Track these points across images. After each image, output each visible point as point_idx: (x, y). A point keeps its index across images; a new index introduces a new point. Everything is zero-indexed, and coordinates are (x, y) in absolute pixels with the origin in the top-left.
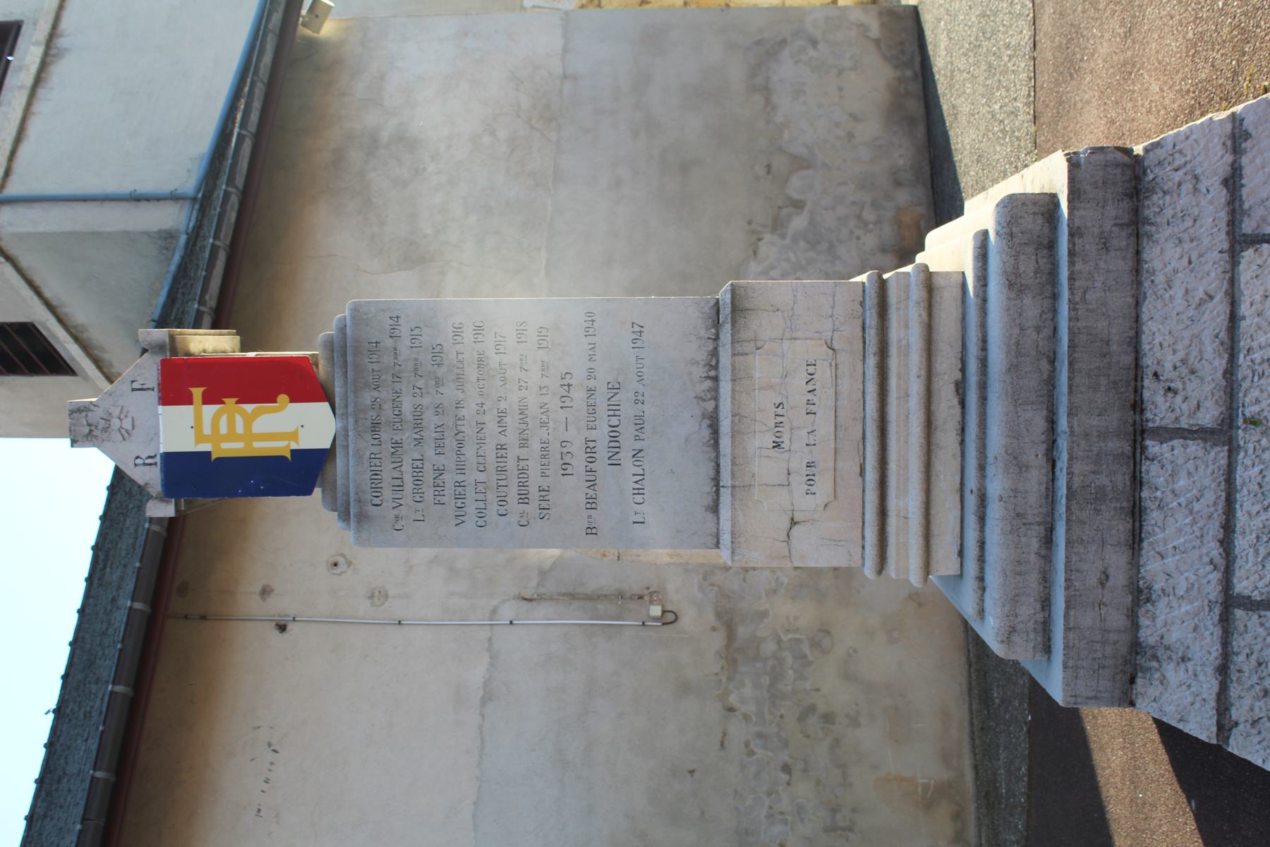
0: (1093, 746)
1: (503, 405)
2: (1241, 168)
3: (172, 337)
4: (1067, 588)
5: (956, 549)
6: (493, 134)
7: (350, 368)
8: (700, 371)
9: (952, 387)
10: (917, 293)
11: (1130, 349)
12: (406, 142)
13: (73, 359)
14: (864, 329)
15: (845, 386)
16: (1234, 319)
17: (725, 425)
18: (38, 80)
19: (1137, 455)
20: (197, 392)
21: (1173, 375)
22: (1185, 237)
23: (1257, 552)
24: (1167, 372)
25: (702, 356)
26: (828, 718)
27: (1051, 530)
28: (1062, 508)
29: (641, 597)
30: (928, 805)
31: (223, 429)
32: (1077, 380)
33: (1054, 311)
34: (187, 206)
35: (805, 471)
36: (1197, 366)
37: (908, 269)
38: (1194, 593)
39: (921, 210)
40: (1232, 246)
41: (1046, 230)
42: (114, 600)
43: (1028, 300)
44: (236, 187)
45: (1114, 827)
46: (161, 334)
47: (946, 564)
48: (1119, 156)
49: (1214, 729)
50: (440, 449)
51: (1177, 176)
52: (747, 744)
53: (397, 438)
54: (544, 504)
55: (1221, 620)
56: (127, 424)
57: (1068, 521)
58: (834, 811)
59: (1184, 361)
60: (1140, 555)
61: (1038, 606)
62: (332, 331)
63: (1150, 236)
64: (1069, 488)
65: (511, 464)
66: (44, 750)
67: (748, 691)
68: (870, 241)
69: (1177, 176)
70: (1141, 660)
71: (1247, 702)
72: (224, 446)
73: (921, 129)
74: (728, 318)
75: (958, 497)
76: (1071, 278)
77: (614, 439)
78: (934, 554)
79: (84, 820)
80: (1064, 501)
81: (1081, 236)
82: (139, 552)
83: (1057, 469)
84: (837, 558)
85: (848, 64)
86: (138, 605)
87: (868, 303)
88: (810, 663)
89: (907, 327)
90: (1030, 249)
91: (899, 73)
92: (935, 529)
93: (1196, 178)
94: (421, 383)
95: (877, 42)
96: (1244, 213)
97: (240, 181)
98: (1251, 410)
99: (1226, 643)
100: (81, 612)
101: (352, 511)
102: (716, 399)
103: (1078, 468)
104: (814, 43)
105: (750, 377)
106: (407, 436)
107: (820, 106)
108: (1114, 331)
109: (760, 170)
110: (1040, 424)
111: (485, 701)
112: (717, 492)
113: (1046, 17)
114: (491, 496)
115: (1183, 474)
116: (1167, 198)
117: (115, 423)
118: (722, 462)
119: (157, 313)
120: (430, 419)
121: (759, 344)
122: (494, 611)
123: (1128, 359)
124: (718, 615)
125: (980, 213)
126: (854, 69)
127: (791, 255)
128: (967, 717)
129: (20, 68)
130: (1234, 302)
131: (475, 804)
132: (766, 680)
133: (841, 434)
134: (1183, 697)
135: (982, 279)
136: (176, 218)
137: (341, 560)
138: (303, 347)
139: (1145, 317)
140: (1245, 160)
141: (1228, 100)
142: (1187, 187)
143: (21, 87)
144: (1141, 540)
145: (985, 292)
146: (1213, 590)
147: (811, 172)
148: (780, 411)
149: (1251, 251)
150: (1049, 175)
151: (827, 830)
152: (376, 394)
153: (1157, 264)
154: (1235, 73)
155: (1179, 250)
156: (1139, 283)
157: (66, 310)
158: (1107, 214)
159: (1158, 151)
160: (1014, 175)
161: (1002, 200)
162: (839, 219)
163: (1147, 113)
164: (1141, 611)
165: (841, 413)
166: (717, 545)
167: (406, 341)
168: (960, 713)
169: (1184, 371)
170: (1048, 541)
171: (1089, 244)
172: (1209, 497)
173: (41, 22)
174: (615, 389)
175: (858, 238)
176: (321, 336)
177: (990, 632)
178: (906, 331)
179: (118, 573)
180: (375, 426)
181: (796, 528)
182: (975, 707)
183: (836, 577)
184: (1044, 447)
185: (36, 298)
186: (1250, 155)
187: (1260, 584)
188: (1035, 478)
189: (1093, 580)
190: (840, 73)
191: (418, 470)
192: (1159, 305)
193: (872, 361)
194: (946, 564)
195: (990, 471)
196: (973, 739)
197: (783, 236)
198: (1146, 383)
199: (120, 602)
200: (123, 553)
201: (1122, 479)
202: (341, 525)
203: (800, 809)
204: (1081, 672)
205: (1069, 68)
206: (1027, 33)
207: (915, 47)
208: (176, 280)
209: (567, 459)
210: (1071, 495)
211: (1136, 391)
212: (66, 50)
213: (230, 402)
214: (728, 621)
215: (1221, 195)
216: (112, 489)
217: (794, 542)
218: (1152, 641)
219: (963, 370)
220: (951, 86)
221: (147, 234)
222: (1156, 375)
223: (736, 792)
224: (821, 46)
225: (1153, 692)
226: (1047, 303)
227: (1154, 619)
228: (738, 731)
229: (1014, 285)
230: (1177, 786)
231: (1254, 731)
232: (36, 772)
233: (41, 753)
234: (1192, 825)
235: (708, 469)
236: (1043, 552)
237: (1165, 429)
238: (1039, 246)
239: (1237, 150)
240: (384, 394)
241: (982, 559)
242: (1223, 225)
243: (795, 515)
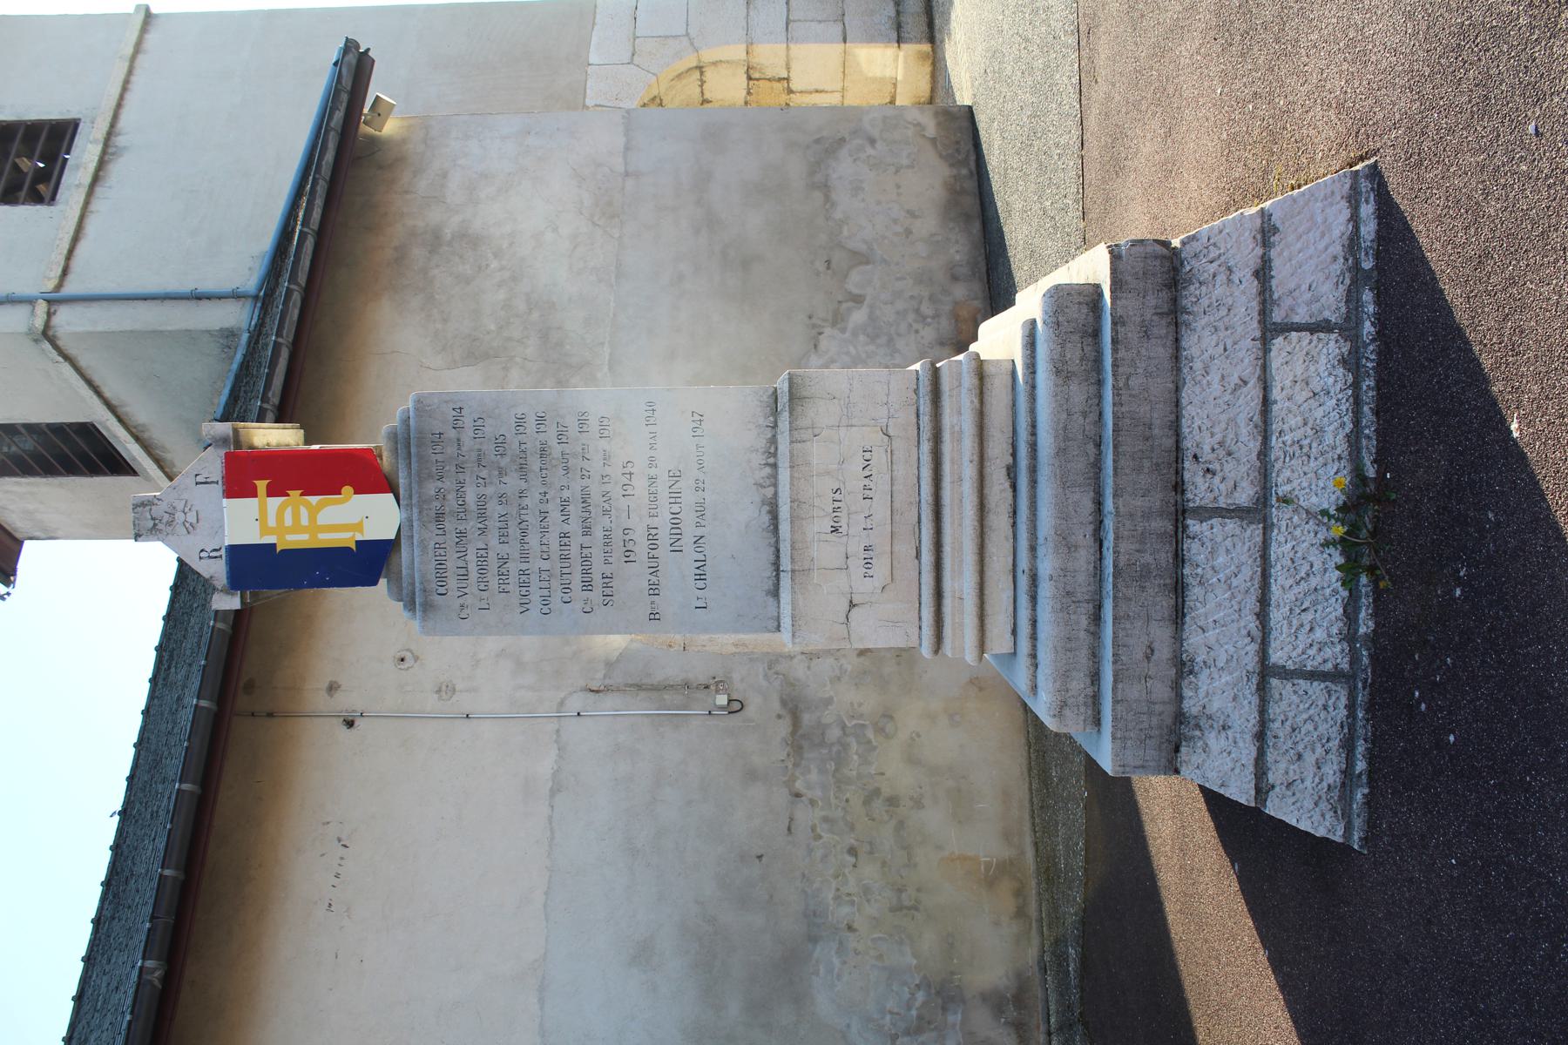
0: (1145, 818)
1: (566, 494)
2: (1270, 260)
3: (236, 431)
4: (1115, 662)
5: (1009, 629)
6: (555, 230)
7: (414, 459)
8: (759, 459)
9: (1004, 471)
10: (969, 381)
12: (470, 240)
13: (134, 459)
15: (900, 471)
16: (1266, 403)
18: (96, 179)
19: (1178, 533)
20: (262, 485)
21: (1211, 457)
22: (1220, 325)
24: (1206, 454)
25: (762, 443)
26: (893, 801)
29: (707, 687)
30: (990, 882)
31: (288, 521)
32: (1122, 462)
33: (1100, 397)
34: (249, 304)
35: (863, 554)
36: (1233, 448)
37: (960, 357)
39: (977, 304)
40: (1264, 334)
41: (1091, 319)
42: (179, 699)
43: (1074, 387)
45: (1164, 893)
46: (225, 428)
47: (1000, 641)
48: (1158, 248)
49: (1253, 792)
50: (504, 538)
51: (1213, 268)
52: (813, 829)
53: (461, 528)
54: (608, 591)
55: (1258, 689)
56: (191, 518)
57: (1115, 598)
59: (1221, 444)
61: (1088, 681)
62: (396, 422)
63: (1188, 325)
64: (1115, 566)
65: (574, 550)
66: (110, 853)
67: (814, 776)
68: (928, 334)
69: (1213, 268)
70: (1184, 730)
71: (1282, 766)
73: (976, 227)
74: (786, 406)
76: (1115, 365)
77: (675, 526)
78: (988, 634)
79: (153, 918)
81: (1124, 324)
82: (204, 650)
85: (905, 162)
86: (204, 703)
88: (875, 748)
89: (960, 413)
90: (1076, 338)
91: (955, 171)
92: (989, 609)
93: (1229, 269)
94: (484, 473)
95: (933, 141)
96: (1274, 302)
97: (302, 279)
98: (1283, 490)
99: (1262, 711)
101: (417, 601)
102: (775, 485)
104: (872, 142)
105: (808, 464)
106: (472, 525)
107: (879, 203)
110: (1087, 505)
111: (553, 792)
112: (778, 577)
113: (1092, 118)
114: (555, 584)
115: (1222, 551)
117: (180, 517)
119: (220, 411)
120: (494, 509)
122: (562, 703)
123: (1169, 442)
124: (784, 703)
125: (1029, 303)
126: (911, 167)
127: (852, 349)
128: (1027, 797)
129: (77, 167)
131: (546, 894)
132: (831, 766)
133: (896, 518)
134: (1223, 763)
135: (1031, 367)
136: (237, 316)
137: (408, 655)
138: (370, 432)
139: (1184, 402)
140: (1273, 253)
141: (1259, 197)
142: (1222, 278)
143: (78, 186)
144: (1184, 615)
146: (1251, 661)
147: (869, 267)
148: (837, 496)
149: (1281, 339)
150: (1093, 267)
152: (439, 484)
153: (1195, 351)
154: (1266, 172)
156: (1179, 370)
157: (128, 409)
159: (1194, 244)
162: (898, 313)
163: (1182, 206)
164: (1185, 683)
166: (778, 629)
167: (467, 436)
168: (1021, 792)
169: (1222, 453)
171: (1131, 333)
172: (1246, 572)
174: (676, 477)
175: (917, 332)
176: (385, 429)
177: (1043, 707)
179: (183, 672)
180: (439, 517)
181: (854, 610)
184: (1091, 527)
186: (1278, 249)
187: (1294, 654)
188: (1084, 558)
190: (897, 171)
191: (482, 559)
192: (1197, 389)
193: (926, 447)
194: (1000, 641)
195: (1041, 551)
196: (1033, 817)
197: (843, 330)
198: (1187, 464)
199: (186, 701)
201: (1165, 557)
202: (406, 614)
203: (866, 891)
205: (1116, 166)
206: (1076, 133)
207: (970, 146)
208: (238, 378)
209: (630, 546)
210: (1117, 573)
213: (295, 494)
214: (793, 707)
215: (1253, 286)
216: (175, 589)
217: (853, 624)
218: (1195, 711)
219: (1014, 455)
224: (879, 145)
225: (1195, 759)
226: (1092, 389)
227: (1197, 689)
229: (1061, 371)
232: (102, 874)
233: (107, 856)
234: (1235, 886)
237: (1205, 509)
238: (1084, 334)
240: (448, 484)
241: (1034, 637)
242: (1255, 315)
243: (856, 603)
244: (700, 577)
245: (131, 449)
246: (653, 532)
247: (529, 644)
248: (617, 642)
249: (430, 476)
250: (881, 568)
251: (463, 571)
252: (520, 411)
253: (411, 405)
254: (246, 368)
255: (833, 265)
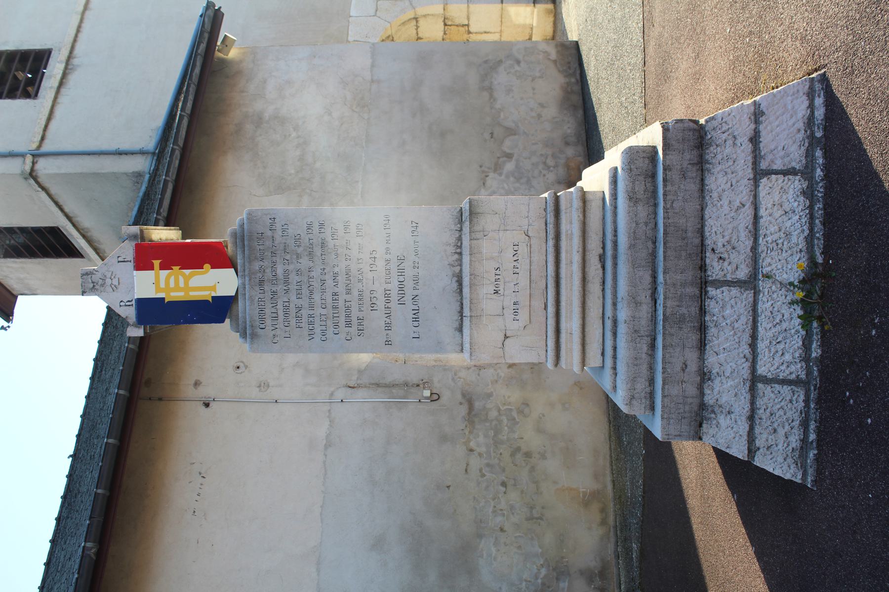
0: (679, 466)
1: (336, 270)
2: (759, 132)
3: (142, 231)
5: (600, 352)
7: (246, 248)
8: (451, 249)
10: (577, 203)
11: (699, 235)
13: (82, 248)
14: (546, 225)
16: (756, 217)
17: (466, 281)
18: (61, 84)
19: (702, 296)
20: (157, 263)
21: (723, 250)
22: (729, 171)
23: (770, 351)
24: (719, 248)
25: (453, 240)
26: (528, 455)
27: (654, 339)
28: (660, 327)
29: (418, 386)
30: (586, 504)
31: (172, 284)
32: (669, 253)
33: (655, 213)
34: (149, 157)
35: (513, 307)
36: (736, 245)
37: (572, 189)
38: (735, 375)
39: (580, 159)
41: (650, 167)
43: (640, 208)
44: (178, 145)
45: (691, 512)
46: (135, 229)
47: (594, 359)
48: (691, 124)
49: (746, 452)
50: (299, 296)
51: (724, 136)
52: (481, 470)
53: (274, 289)
54: (361, 328)
55: (750, 390)
56: (115, 282)
57: (664, 334)
58: (532, 508)
59: (729, 242)
60: (704, 354)
61: (647, 384)
62: (236, 226)
63: (709, 170)
64: (664, 315)
65: (341, 303)
67: (481, 439)
68: (551, 177)
69: (724, 136)
70: (705, 414)
71: (765, 436)
72: (173, 294)
73: (580, 113)
74: (467, 219)
75: (601, 321)
76: (665, 195)
77: (401, 289)
79: (91, 518)
80: (661, 323)
81: (670, 170)
83: (658, 305)
84: (531, 357)
85: (538, 74)
86: (121, 392)
87: (549, 210)
89: (571, 223)
90: (641, 178)
91: (567, 80)
93: (735, 137)
94: (288, 257)
95: (555, 62)
97: (181, 142)
99: (753, 403)
100: (88, 397)
102: (461, 265)
103: (669, 303)
104: (518, 62)
106: (280, 288)
107: (522, 99)
108: (689, 225)
109: (487, 136)
110: (648, 279)
111: (328, 446)
112: (462, 320)
113: (651, 47)
114: (330, 323)
115: (729, 306)
116: (719, 148)
117: (108, 281)
118: (464, 302)
120: (294, 278)
121: (486, 233)
122: (332, 394)
123: (697, 241)
124: (464, 395)
125: (613, 157)
126: (541, 77)
127: (505, 185)
128: (608, 453)
129: (50, 77)
130: (756, 209)
132: (492, 433)
133: (533, 285)
136: (143, 164)
137: (241, 365)
138: (220, 233)
139: (707, 217)
140: (761, 127)
141: (752, 94)
143: (51, 88)
144: (705, 345)
145: (616, 203)
146: (746, 373)
147: (516, 137)
148: (498, 272)
149: (765, 179)
150: (651, 136)
151: (527, 519)
152: (262, 263)
154: (756, 79)
155: (725, 178)
156: (703, 198)
157: (78, 219)
158: (685, 158)
160: (633, 134)
161: (625, 150)
162: (533, 164)
163: (706, 101)
164: (706, 386)
165: (534, 273)
166: (462, 350)
168: (605, 449)
170: (653, 346)
171: (675, 175)
172: (743, 319)
173: (63, 49)
174: (401, 260)
175: (544, 175)
177: (620, 399)
178: (571, 225)
179: (110, 374)
180: (261, 282)
181: (507, 340)
182: (613, 447)
183: (532, 373)
185: (60, 212)
186: (764, 125)
187: (772, 369)
188: (645, 310)
189: (678, 368)
190: (533, 80)
191: (286, 308)
192: (714, 209)
193: (551, 243)
194: (594, 359)
195: (619, 306)
196: (612, 465)
197: (500, 174)
198: (708, 254)
200: (112, 362)
201: (695, 310)
202: (241, 340)
203: (512, 508)
204: (672, 421)
205: (665, 76)
206: (640, 56)
207: (577, 65)
208: (143, 201)
209: (374, 301)
211: (702, 259)
212: (78, 66)
213: (176, 268)
214: (469, 400)
215: (749, 147)
217: (506, 348)
218: (711, 402)
219: (604, 248)
220: (597, 88)
221: (126, 174)
222: (713, 250)
223: (474, 498)
224: (522, 64)
225: (712, 431)
226: (651, 209)
227: (713, 390)
228: (475, 463)
229: (632, 198)
230: (726, 487)
231: (769, 453)
232: (61, 492)
233: (64, 481)
235: (456, 307)
236: (650, 353)
237: (719, 281)
239: (757, 122)
240: (266, 263)
241: (615, 357)
242: (750, 164)
243: (506, 335)
244: (416, 320)
245: (80, 242)
246: (388, 292)
247: (313, 358)
248: (365, 358)
249: (256, 258)
250: (523, 315)
251: (275, 315)
252: (309, 220)
253: (245, 216)
254: (147, 197)
255: (495, 135)
